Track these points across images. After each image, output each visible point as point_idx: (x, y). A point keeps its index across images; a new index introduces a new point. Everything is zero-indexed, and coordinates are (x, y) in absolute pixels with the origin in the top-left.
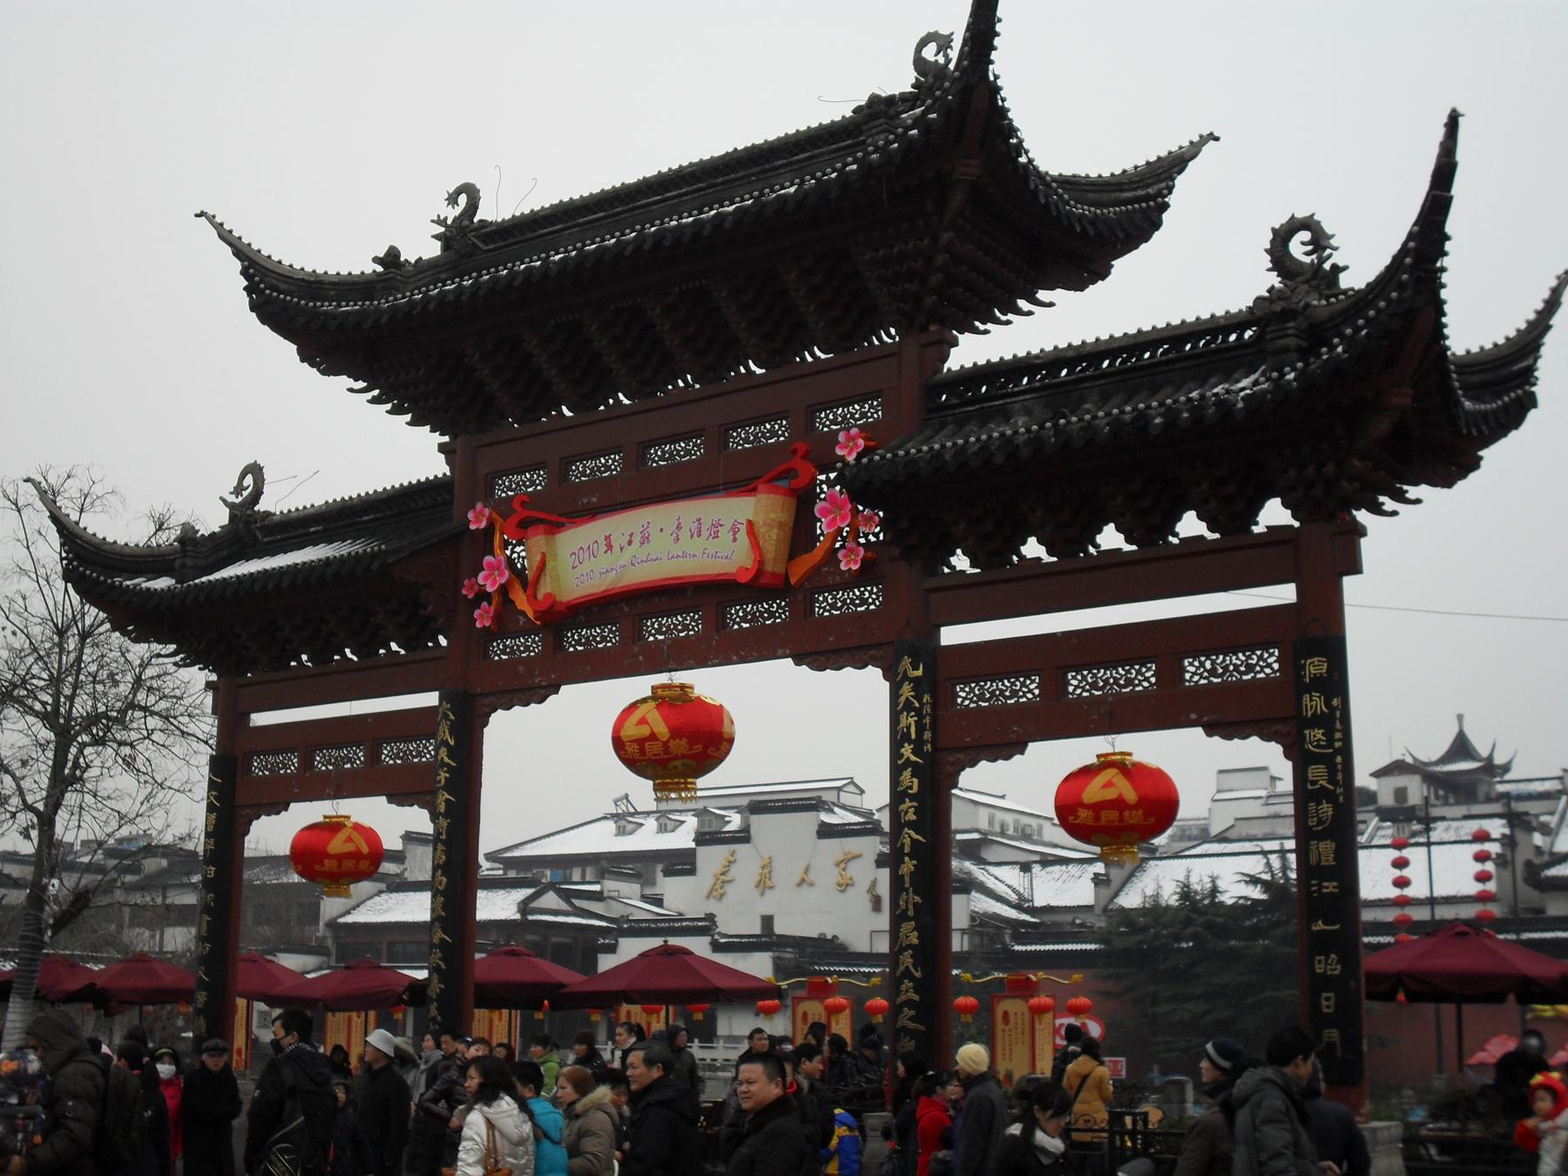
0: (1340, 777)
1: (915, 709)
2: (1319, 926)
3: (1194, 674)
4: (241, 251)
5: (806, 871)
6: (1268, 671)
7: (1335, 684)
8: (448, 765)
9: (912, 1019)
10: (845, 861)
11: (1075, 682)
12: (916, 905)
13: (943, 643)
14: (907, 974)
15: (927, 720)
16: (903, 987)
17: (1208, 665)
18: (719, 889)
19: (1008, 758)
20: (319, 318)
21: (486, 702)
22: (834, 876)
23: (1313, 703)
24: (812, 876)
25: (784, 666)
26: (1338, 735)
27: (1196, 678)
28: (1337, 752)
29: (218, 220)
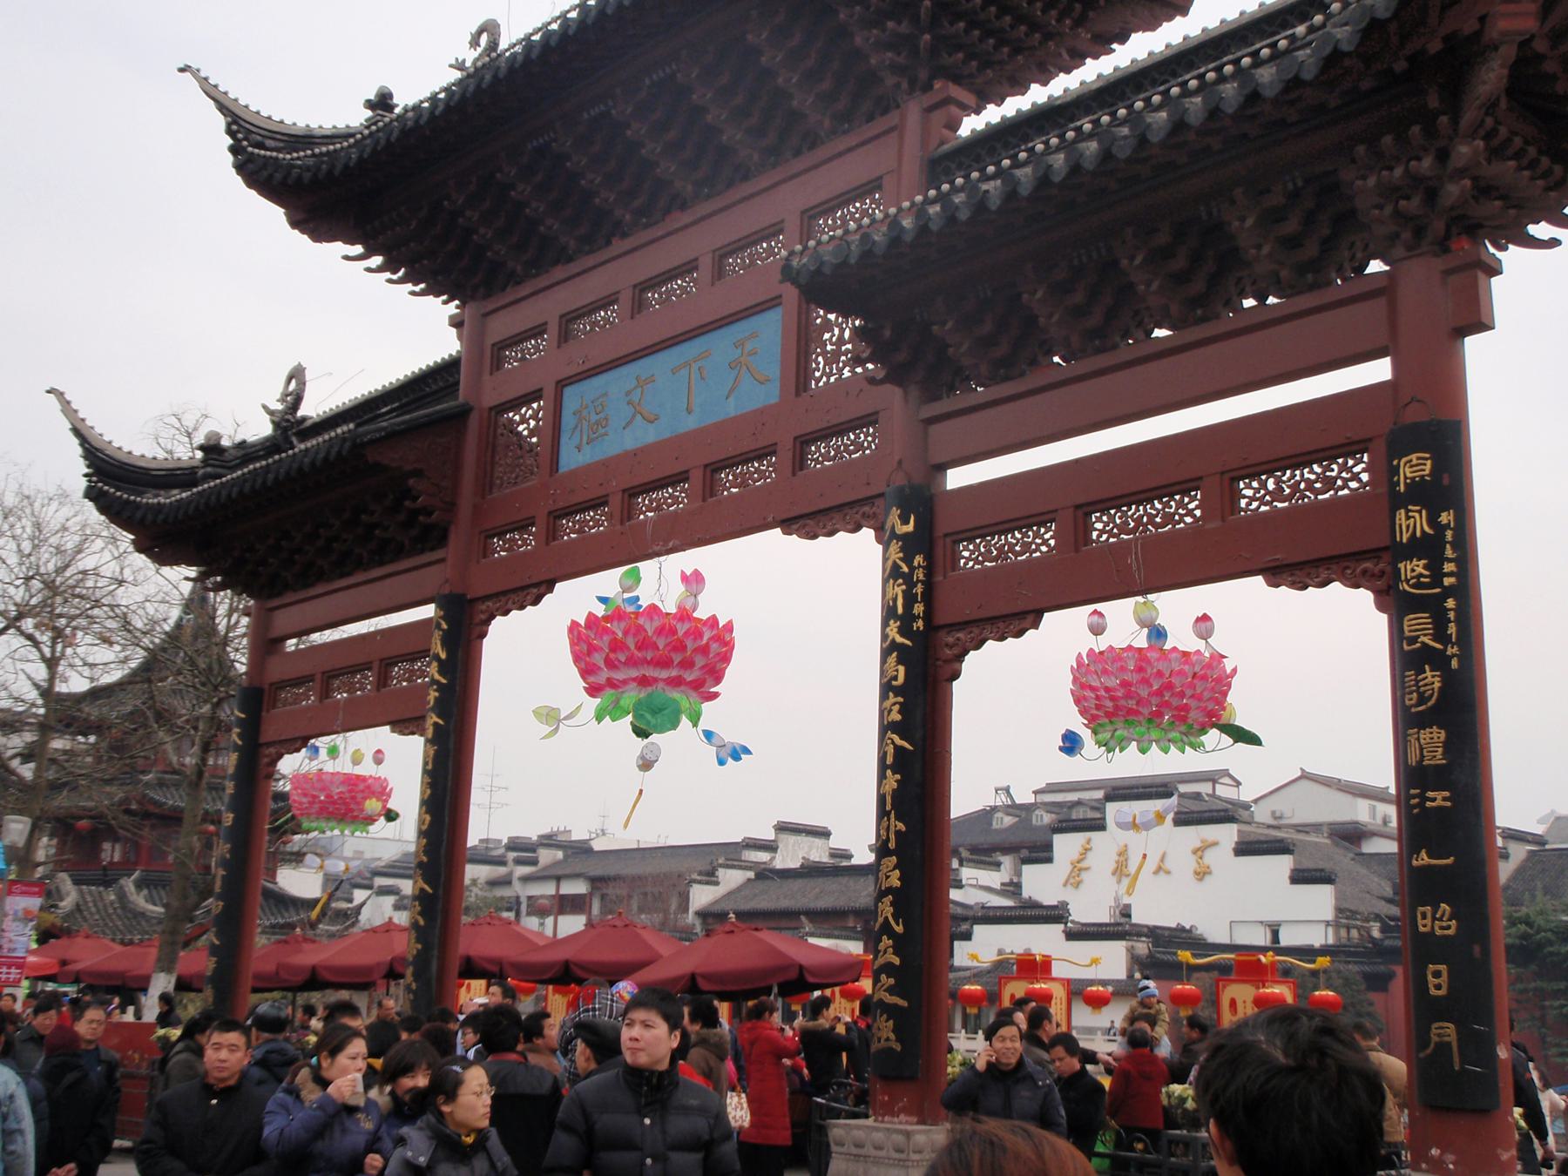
0: (1452, 629)
1: (903, 575)
2: (1423, 859)
3: (1252, 499)
4: (224, 106)
5: (1162, 859)
6: (1354, 485)
7: (1448, 489)
8: (437, 682)
9: (890, 990)
10: (1199, 851)
11: (1099, 526)
12: (898, 833)
13: (949, 487)
14: (886, 928)
15: (919, 589)
16: (882, 946)
17: (1271, 485)
18: (1075, 878)
19: (1019, 634)
20: (335, 185)
21: (483, 607)
22: (1191, 863)
23: (1412, 522)
24: (1168, 865)
25: (774, 536)
26: (1449, 567)
27: (1255, 505)
28: (1448, 592)
29: (203, 74)
